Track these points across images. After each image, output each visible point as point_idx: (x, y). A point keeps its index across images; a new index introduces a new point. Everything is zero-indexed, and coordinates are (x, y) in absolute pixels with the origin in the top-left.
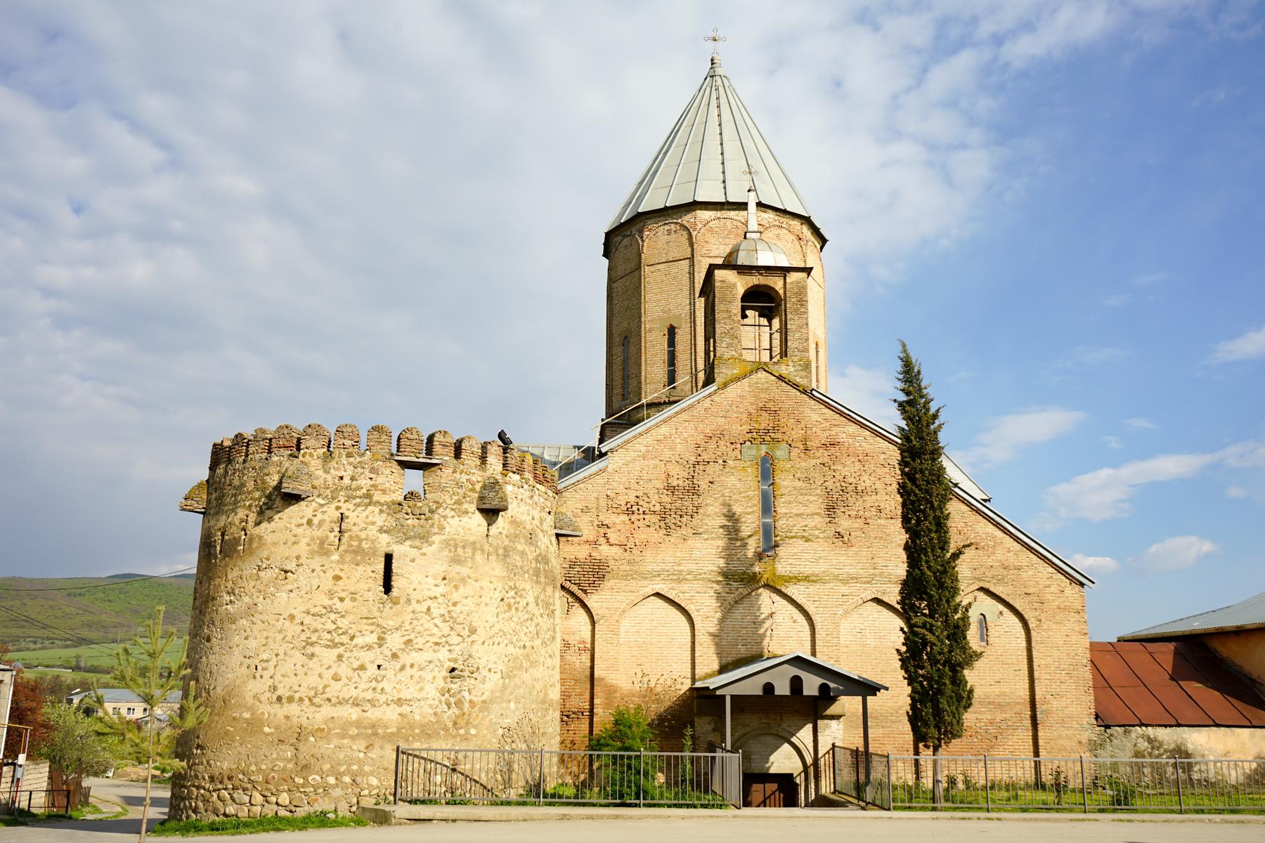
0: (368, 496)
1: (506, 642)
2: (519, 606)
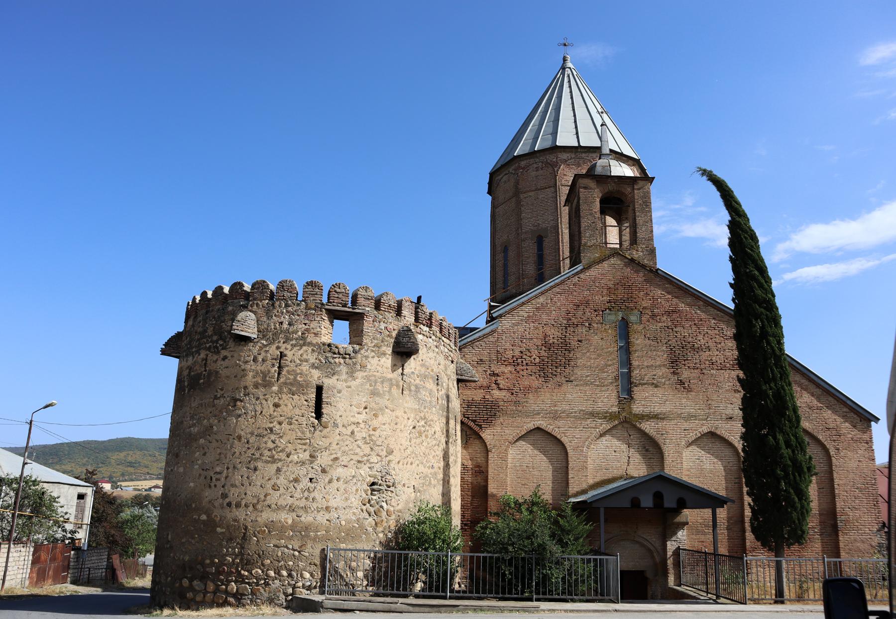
0: (303, 338)
1: (417, 462)
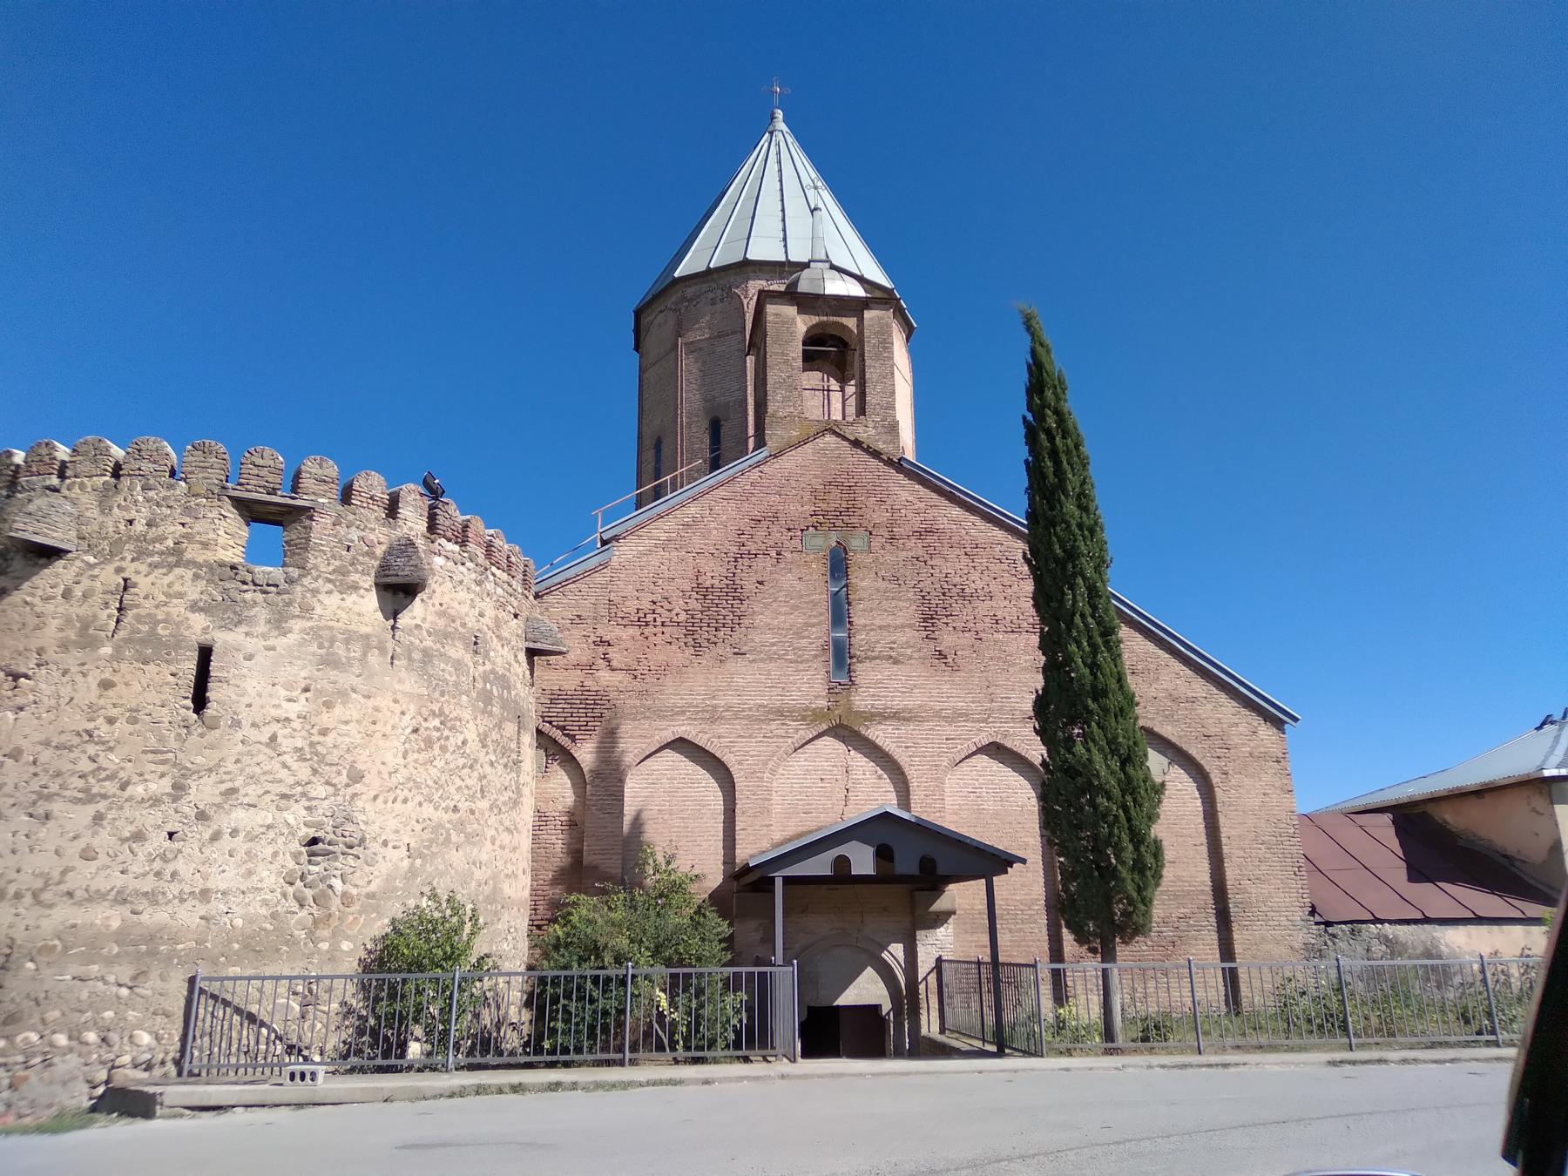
0: (177, 551)
1: (420, 798)
2: (448, 743)
